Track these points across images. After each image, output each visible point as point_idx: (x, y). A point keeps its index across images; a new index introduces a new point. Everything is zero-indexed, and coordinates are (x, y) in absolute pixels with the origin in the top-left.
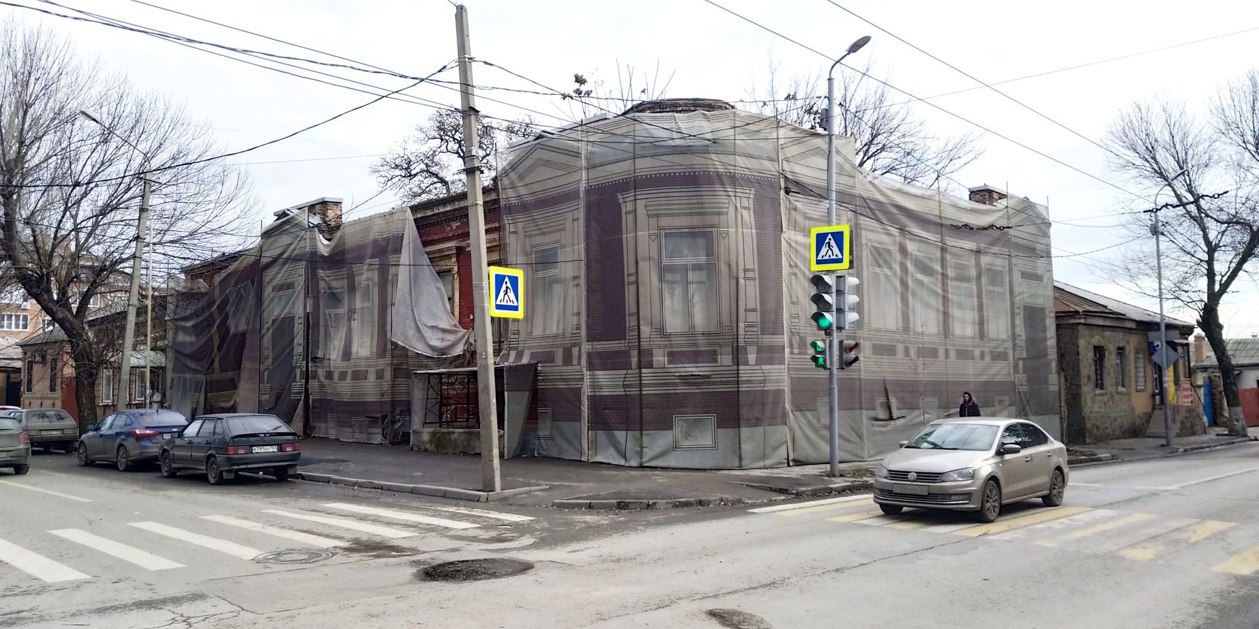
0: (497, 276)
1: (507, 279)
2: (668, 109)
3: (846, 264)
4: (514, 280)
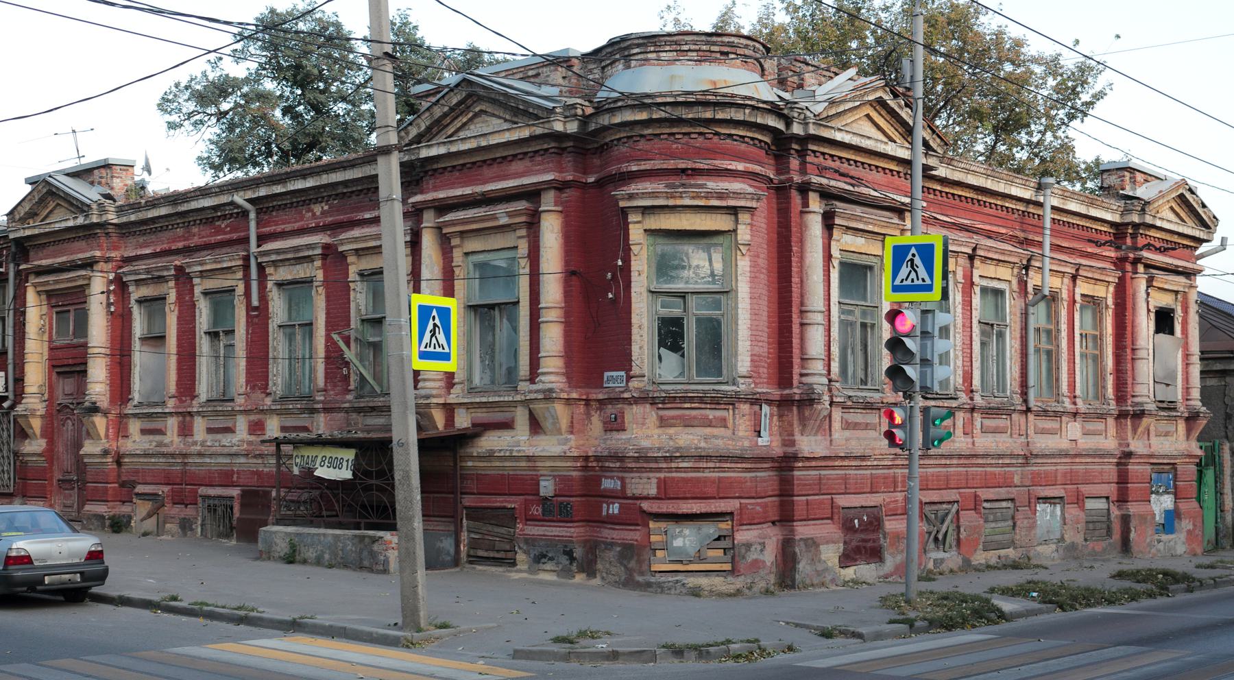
0: (421, 307)
1: (434, 313)
2: (668, 48)
3: (936, 294)
4: (444, 313)
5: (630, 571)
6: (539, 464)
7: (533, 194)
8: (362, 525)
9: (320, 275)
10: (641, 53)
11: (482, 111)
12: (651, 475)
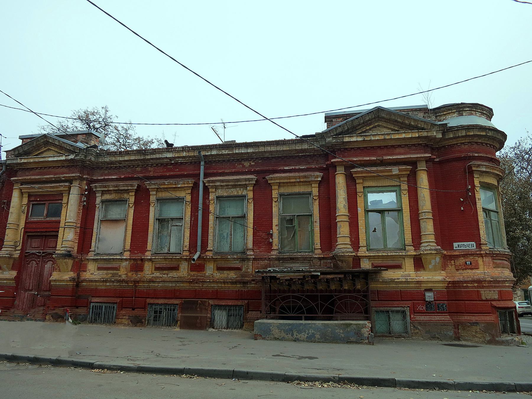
5: (493, 336)
6: (422, 285)
7: (414, 163)
8: (303, 318)
9: (251, 195)
10: (469, 110)
11: (379, 126)
12: (495, 289)
